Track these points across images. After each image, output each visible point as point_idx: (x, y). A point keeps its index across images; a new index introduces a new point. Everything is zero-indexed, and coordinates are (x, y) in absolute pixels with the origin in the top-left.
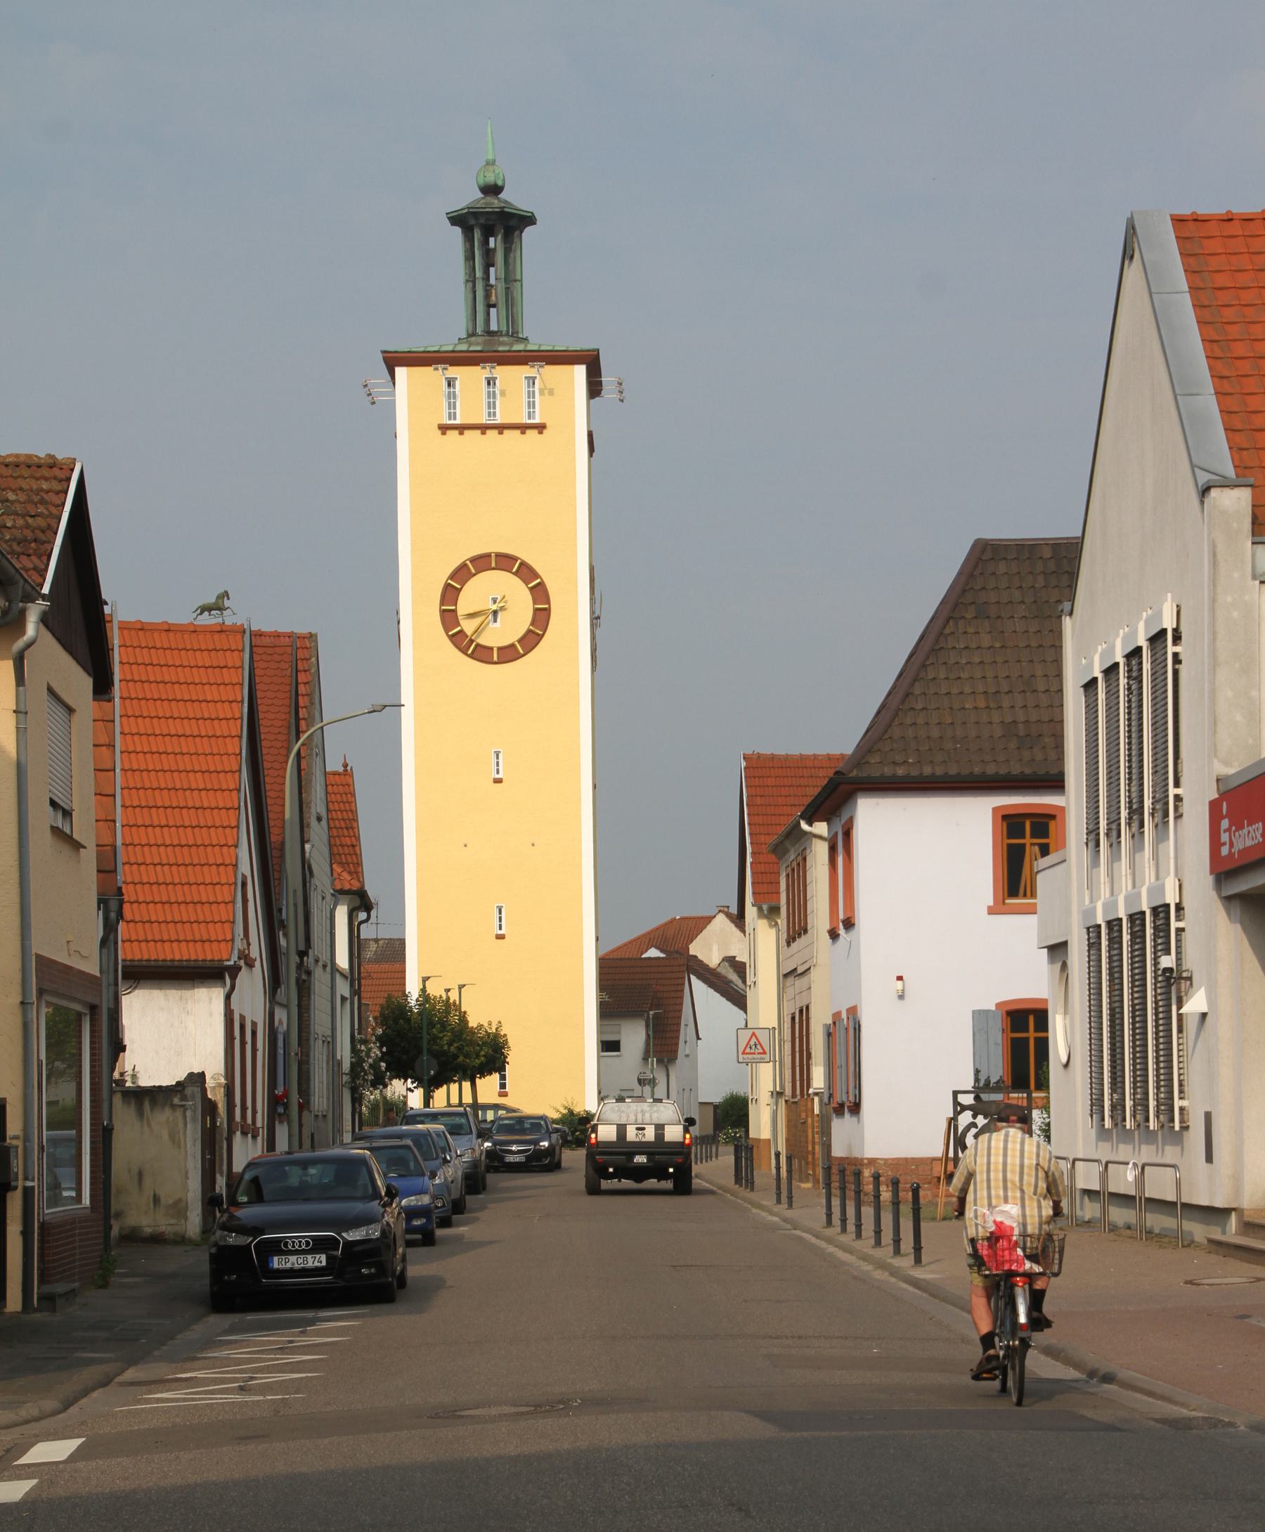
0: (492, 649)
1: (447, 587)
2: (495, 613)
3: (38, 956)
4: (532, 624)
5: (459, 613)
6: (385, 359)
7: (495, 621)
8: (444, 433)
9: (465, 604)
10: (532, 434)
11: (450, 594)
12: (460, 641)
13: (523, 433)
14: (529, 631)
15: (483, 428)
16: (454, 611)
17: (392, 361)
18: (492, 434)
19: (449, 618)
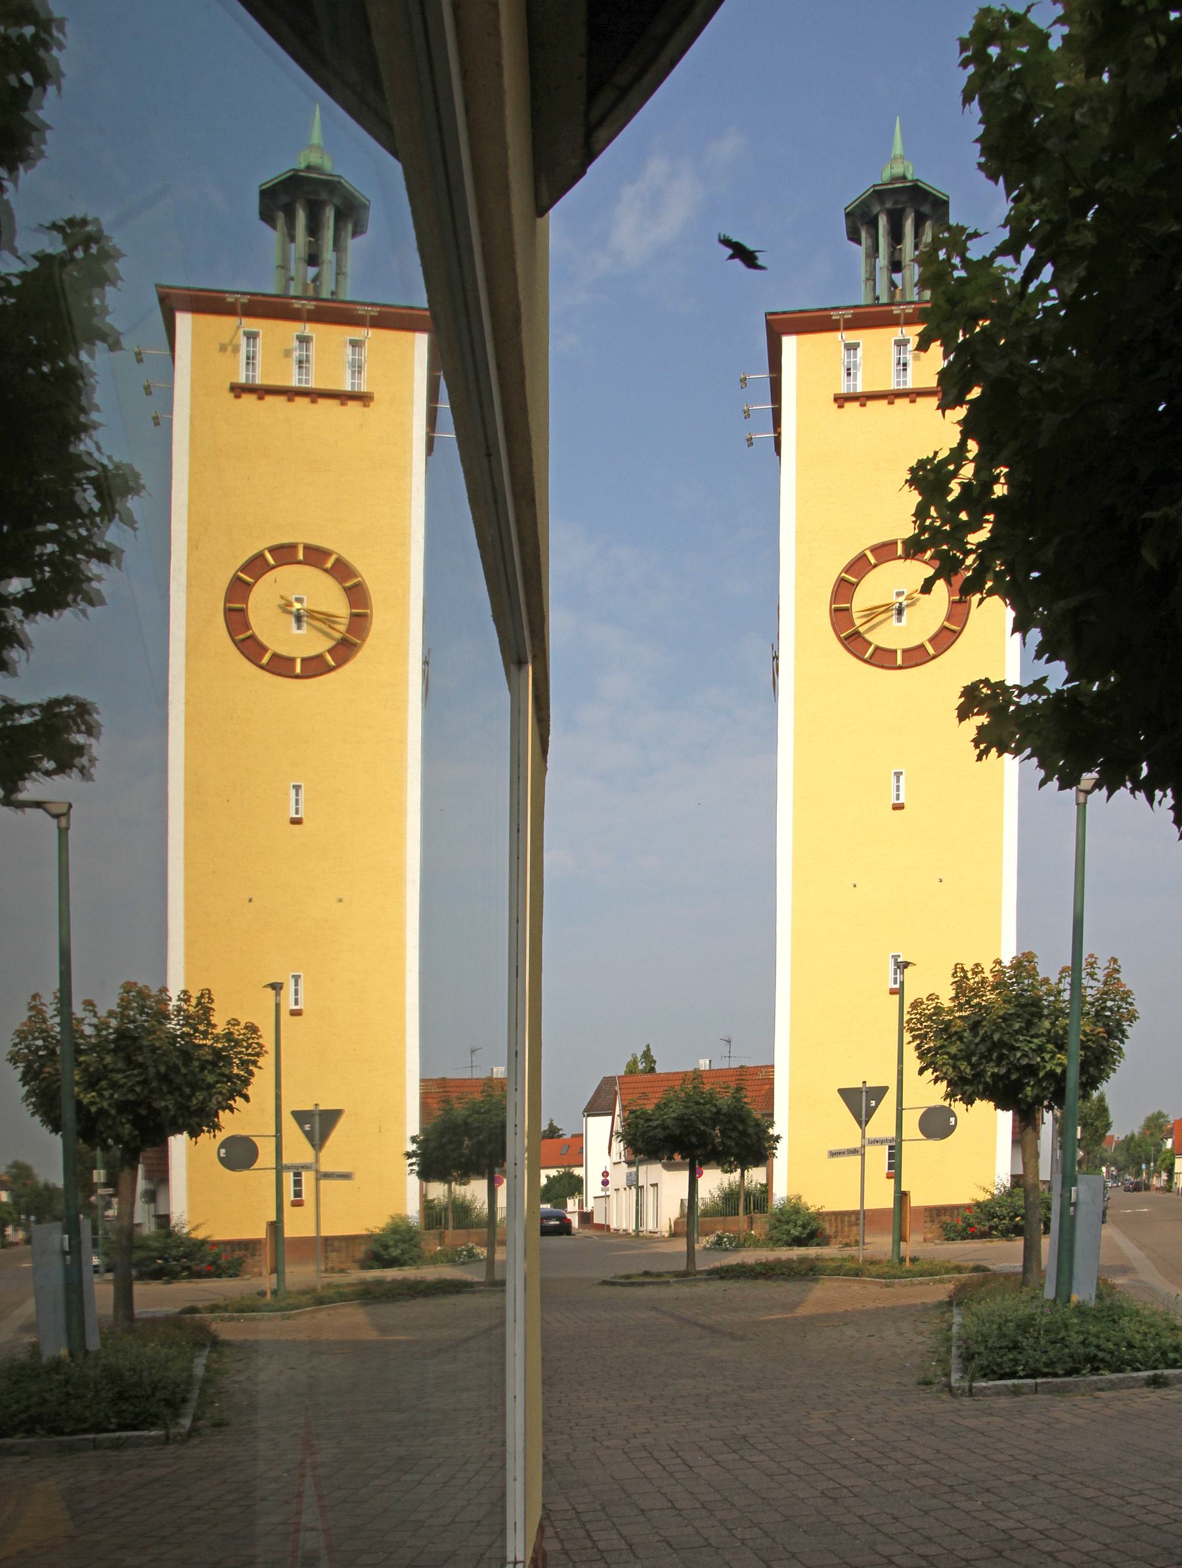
0: (895, 651)
1: (841, 581)
2: (900, 612)
3: (860, 244)
4: (948, 619)
5: (854, 609)
6: (769, 324)
7: (899, 620)
8: (238, 397)
9: (866, 596)
10: (353, 405)
11: (844, 589)
12: (853, 642)
13: (261, 398)
14: (944, 628)
15: (891, 396)
16: (847, 610)
17: (778, 327)
18: (302, 402)
19: (840, 615)
